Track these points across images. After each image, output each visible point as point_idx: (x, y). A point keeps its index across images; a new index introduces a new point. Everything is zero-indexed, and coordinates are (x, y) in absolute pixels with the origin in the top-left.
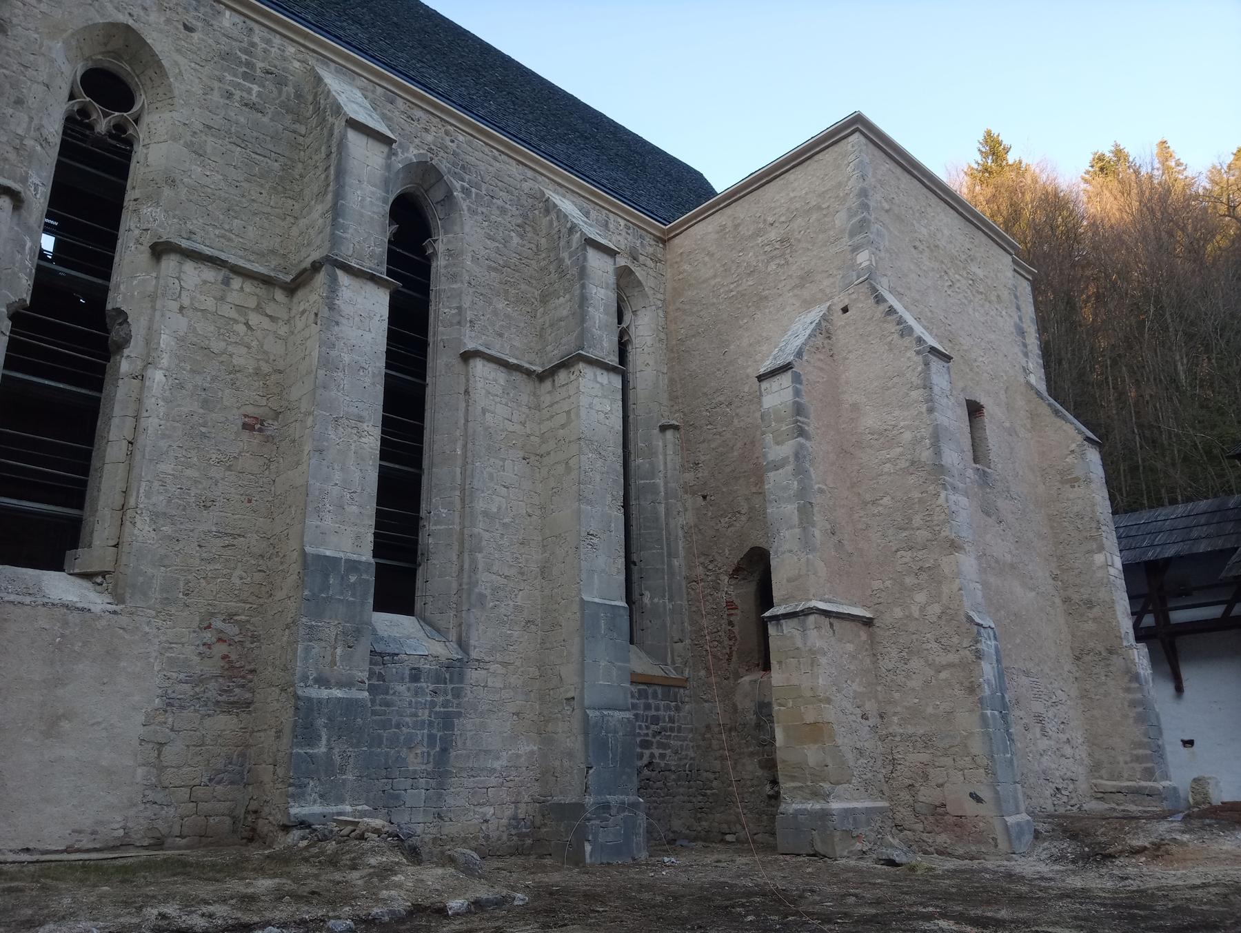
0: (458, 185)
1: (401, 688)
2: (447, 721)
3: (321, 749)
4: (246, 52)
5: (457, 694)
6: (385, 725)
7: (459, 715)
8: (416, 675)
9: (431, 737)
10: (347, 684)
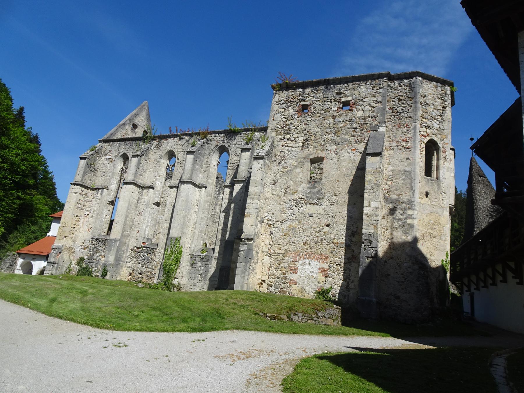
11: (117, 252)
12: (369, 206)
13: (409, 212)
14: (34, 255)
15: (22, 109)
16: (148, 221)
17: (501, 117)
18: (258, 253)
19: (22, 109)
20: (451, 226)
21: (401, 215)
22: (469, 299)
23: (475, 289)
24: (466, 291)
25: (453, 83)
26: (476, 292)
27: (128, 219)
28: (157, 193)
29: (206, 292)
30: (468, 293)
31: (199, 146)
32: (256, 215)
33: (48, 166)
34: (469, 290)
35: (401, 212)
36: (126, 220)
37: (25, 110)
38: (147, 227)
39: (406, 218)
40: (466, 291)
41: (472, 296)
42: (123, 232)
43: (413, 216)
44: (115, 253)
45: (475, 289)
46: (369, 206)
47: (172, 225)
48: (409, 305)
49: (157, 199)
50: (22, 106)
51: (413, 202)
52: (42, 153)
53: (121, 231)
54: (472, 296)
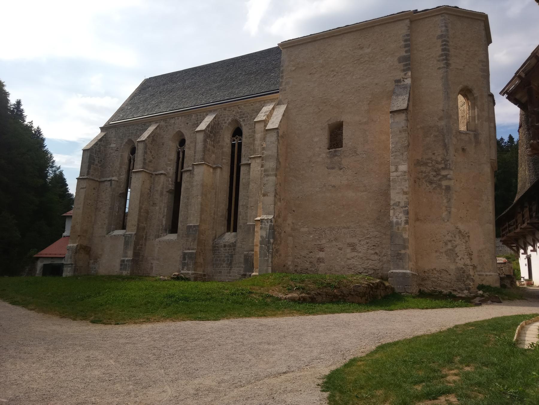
0: (241, 120)
1: (222, 249)
2: (232, 256)
3: (186, 261)
4: (197, 121)
5: (234, 249)
6: (219, 257)
7: (235, 254)
8: (225, 246)
9: (228, 259)
10: (193, 249)
11: (135, 249)
12: (396, 170)
13: (444, 173)
14: (52, 258)
15: (19, 103)
16: (164, 211)
17: (532, 54)
18: (280, 234)
19: (19, 103)
20: (517, 180)
21: (435, 177)
22: (526, 261)
23: (531, 251)
24: (522, 254)
25: (481, 20)
26: (533, 254)
27: (142, 211)
28: (170, 179)
29: (178, 236)
30: (525, 256)
31: (143, 286)
32: (273, 194)
33: (54, 161)
34: (525, 253)
35: (434, 173)
36: (140, 212)
37: (22, 103)
38: (163, 217)
39: (440, 180)
40: (522, 254)
41: (529, 259)
42: (138, 224)
43: (448, 176)
44: (132, 248)
45: (531, 251)
46: (396, 170)
47: (483, 33)
48: (450, 274)
49: (170, 186)
50: (19, 99)
51: (448, 160)
52: (46, 148)
53: (136, 224)
54: (529, 259)
